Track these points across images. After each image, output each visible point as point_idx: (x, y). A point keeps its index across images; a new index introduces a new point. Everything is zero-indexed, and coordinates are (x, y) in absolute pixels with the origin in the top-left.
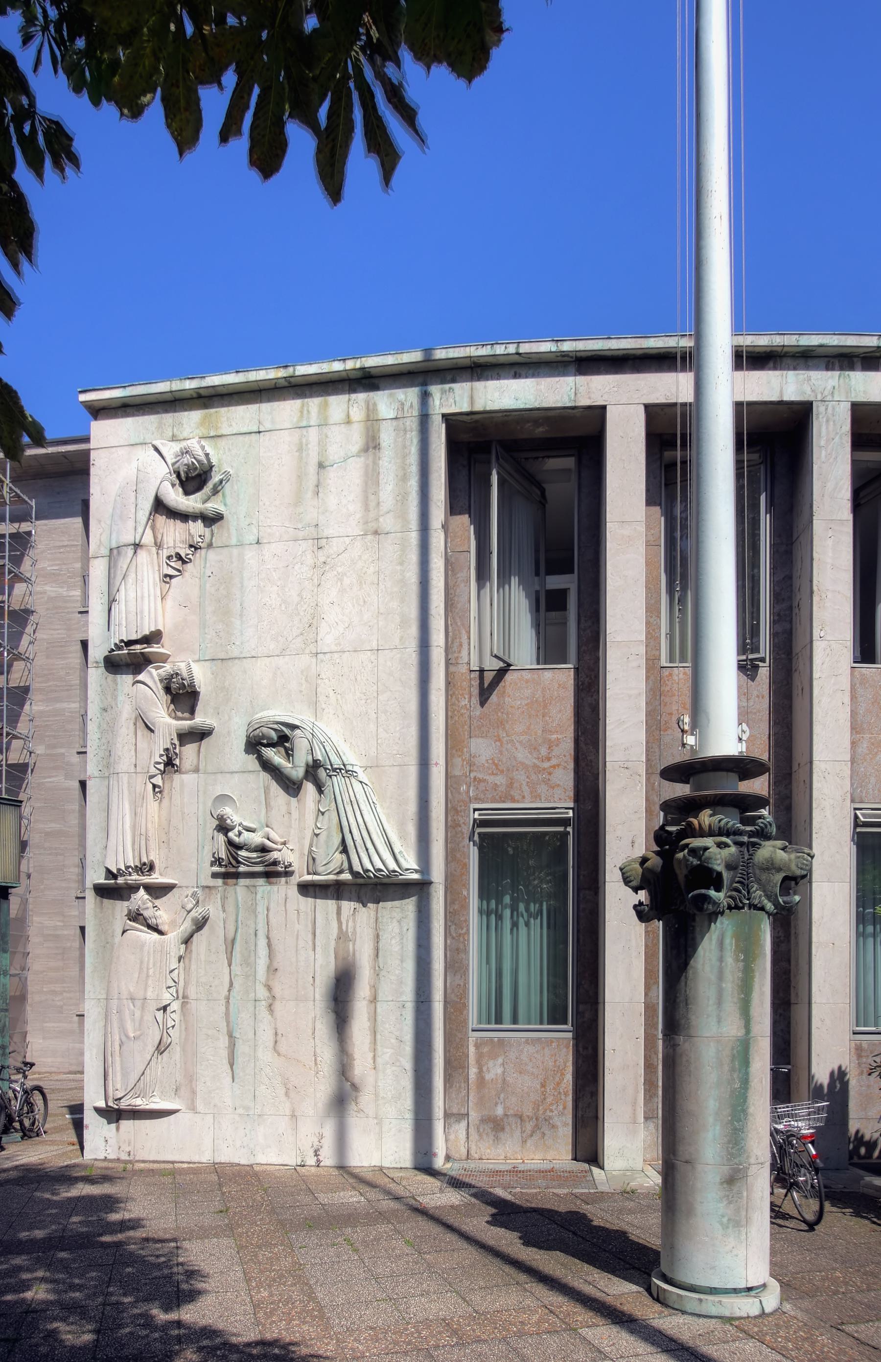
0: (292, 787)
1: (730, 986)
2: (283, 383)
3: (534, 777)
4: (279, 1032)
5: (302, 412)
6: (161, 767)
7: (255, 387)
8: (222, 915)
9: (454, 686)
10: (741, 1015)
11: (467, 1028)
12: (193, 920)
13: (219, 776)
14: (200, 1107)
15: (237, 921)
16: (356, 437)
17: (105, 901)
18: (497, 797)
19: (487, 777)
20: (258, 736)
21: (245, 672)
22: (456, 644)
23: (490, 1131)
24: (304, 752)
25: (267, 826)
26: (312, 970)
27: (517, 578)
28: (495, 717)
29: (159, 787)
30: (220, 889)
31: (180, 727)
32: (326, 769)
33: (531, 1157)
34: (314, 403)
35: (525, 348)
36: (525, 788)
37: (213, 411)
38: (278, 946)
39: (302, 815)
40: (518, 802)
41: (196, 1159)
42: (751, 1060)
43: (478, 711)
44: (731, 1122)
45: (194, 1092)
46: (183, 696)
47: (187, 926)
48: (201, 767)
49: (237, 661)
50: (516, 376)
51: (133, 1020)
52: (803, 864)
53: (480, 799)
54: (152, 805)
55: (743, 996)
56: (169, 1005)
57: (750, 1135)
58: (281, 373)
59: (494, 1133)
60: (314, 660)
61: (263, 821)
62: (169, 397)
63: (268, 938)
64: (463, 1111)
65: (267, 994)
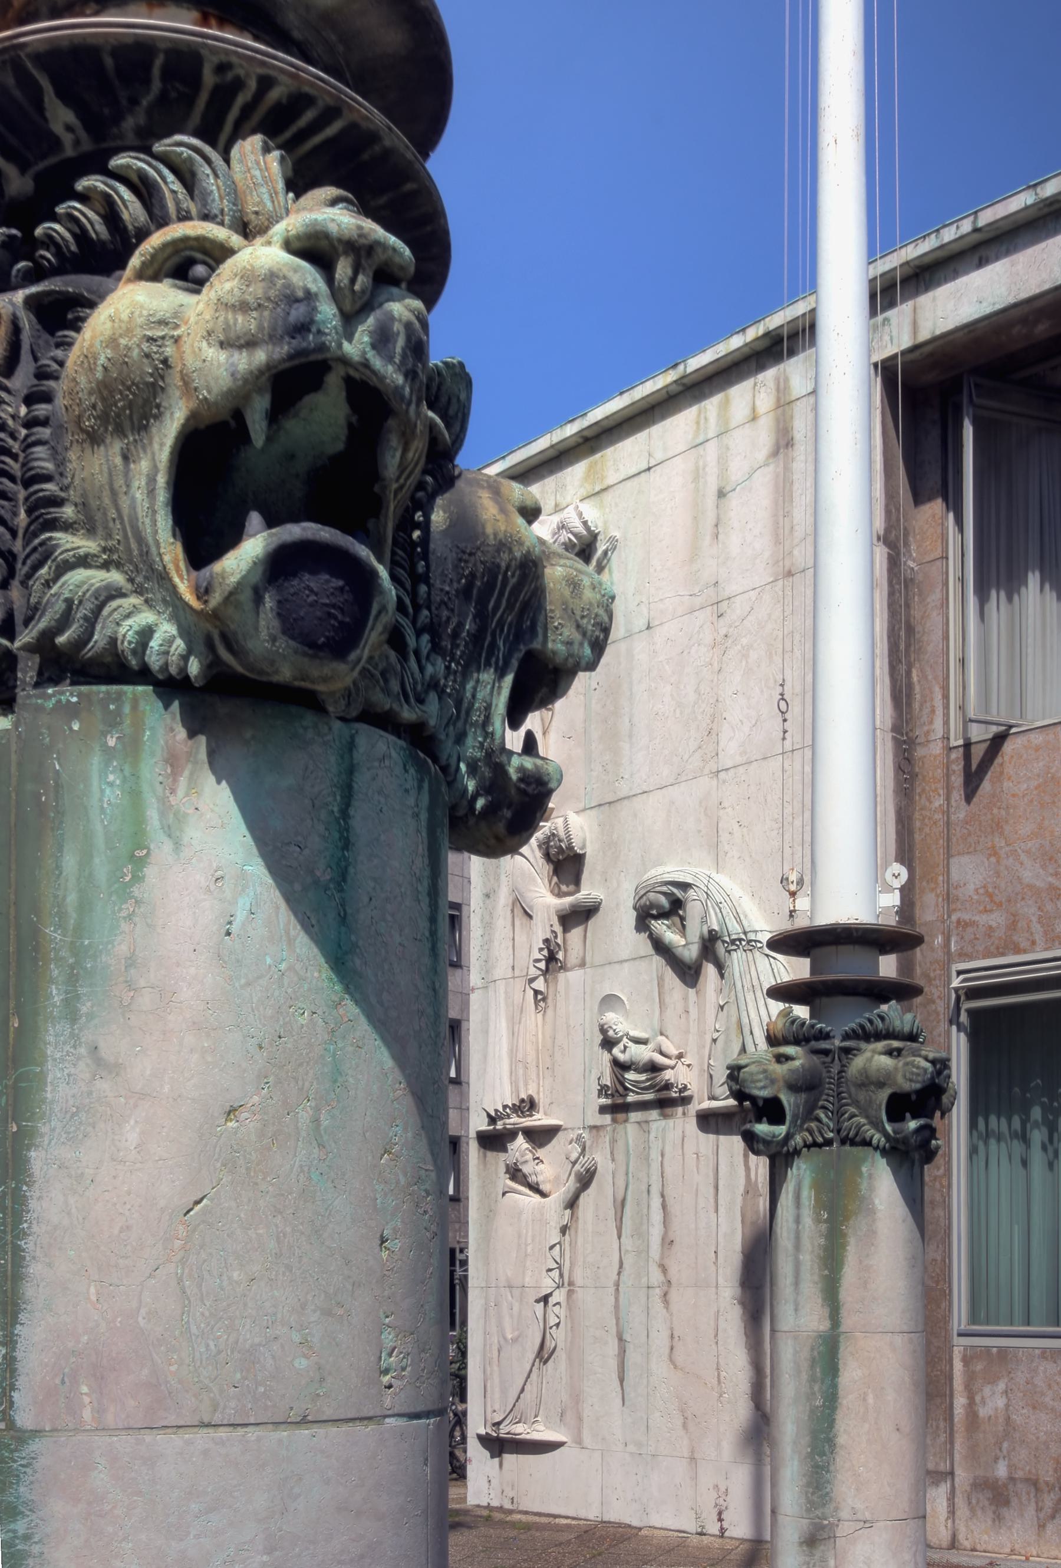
0: (688, 973)
1: (809, 1259)
2: (675, 388)
3: (1049, 907)
4: (676, 1335)
5: (698, 423)
6: (542, 965)
7: (644, 405)
8: (611, 1166)
9: (924, 777)
10: (824, 1300)
11: (947, 1332)
12: (576, 1175)
13: (607, 968)
14: (587, 1440)
15: (627, 1174)
16: (764, 435)
17: (489, 1154)
18: (992, 949)
19: (977, 918)
20: (645, 905)
21: (635, 816)
22: (926, 711)
23: (987, 1503)
24: (698, 920)
25: (662, 1034)
26: (714, 1242)
27: (1037, 574)
28: (989, 816)
29: (541, 993)
30: (608, 1128)
31: (560, 907)
32: (724, 942)
33: (1054, 1553)
34: (712, 405)
35: (986, 217)
36: (1037, 928)
37: (598, 456)
38: (674, 1208)
39: (702, 1012)
40: (1025, 951)
41: (582, 1514)
42: (841, 1366)
43: (961, 811)
44: (811, 1456)
45: (580, 1419)
46: (566, 865)
47: (572, 1184)
48: (588, 959)
49: (626, 802)
50: (982, 263)
51: (511, 1316)
52: (912, 1073)
53: (966, 955)
54: (532, 1019)
55: (826, 1272)
56: (551, 1294)
57: (839, 1476)
58: (671, 377)
59: (993, 1508)
60: (715, 782)
61: (657, 1027)
62: (552, 453)
63: (663, 1196)
64: (944, 1467)
65: (661, 1278)
